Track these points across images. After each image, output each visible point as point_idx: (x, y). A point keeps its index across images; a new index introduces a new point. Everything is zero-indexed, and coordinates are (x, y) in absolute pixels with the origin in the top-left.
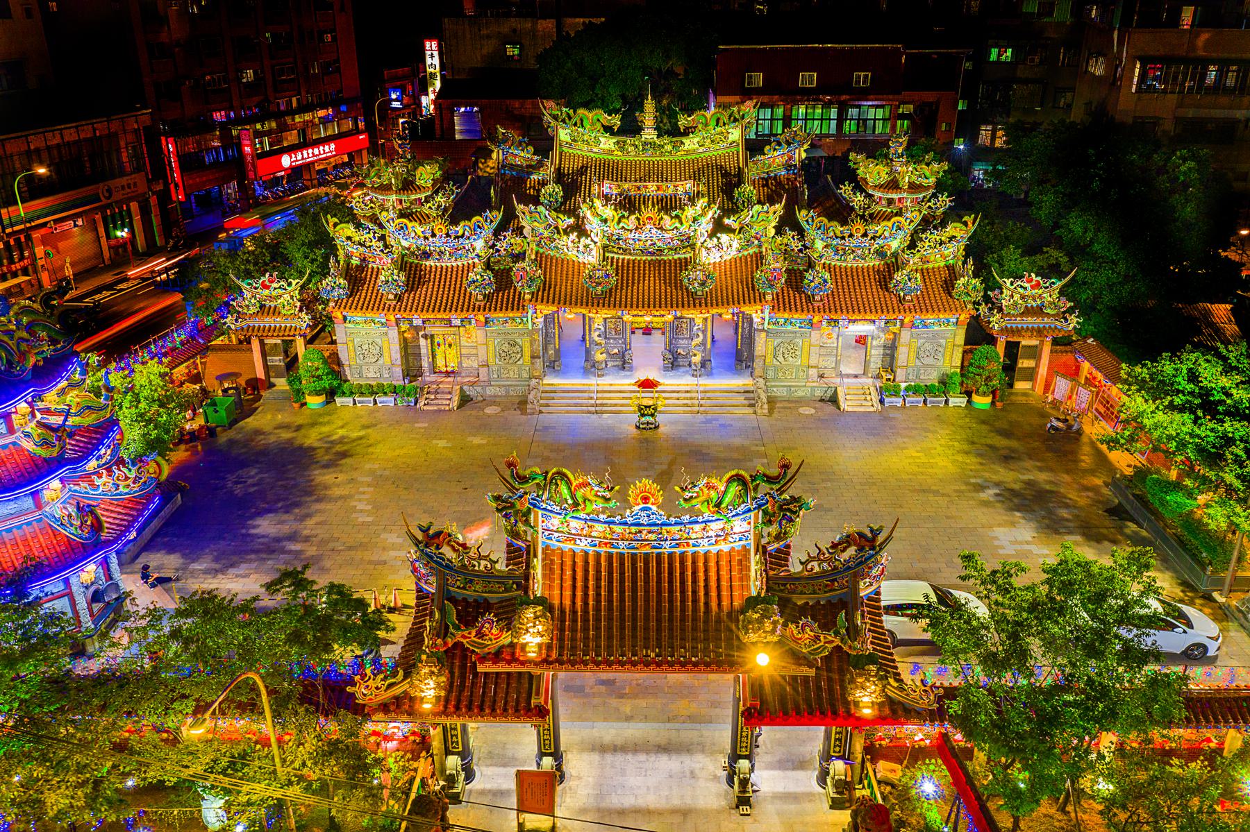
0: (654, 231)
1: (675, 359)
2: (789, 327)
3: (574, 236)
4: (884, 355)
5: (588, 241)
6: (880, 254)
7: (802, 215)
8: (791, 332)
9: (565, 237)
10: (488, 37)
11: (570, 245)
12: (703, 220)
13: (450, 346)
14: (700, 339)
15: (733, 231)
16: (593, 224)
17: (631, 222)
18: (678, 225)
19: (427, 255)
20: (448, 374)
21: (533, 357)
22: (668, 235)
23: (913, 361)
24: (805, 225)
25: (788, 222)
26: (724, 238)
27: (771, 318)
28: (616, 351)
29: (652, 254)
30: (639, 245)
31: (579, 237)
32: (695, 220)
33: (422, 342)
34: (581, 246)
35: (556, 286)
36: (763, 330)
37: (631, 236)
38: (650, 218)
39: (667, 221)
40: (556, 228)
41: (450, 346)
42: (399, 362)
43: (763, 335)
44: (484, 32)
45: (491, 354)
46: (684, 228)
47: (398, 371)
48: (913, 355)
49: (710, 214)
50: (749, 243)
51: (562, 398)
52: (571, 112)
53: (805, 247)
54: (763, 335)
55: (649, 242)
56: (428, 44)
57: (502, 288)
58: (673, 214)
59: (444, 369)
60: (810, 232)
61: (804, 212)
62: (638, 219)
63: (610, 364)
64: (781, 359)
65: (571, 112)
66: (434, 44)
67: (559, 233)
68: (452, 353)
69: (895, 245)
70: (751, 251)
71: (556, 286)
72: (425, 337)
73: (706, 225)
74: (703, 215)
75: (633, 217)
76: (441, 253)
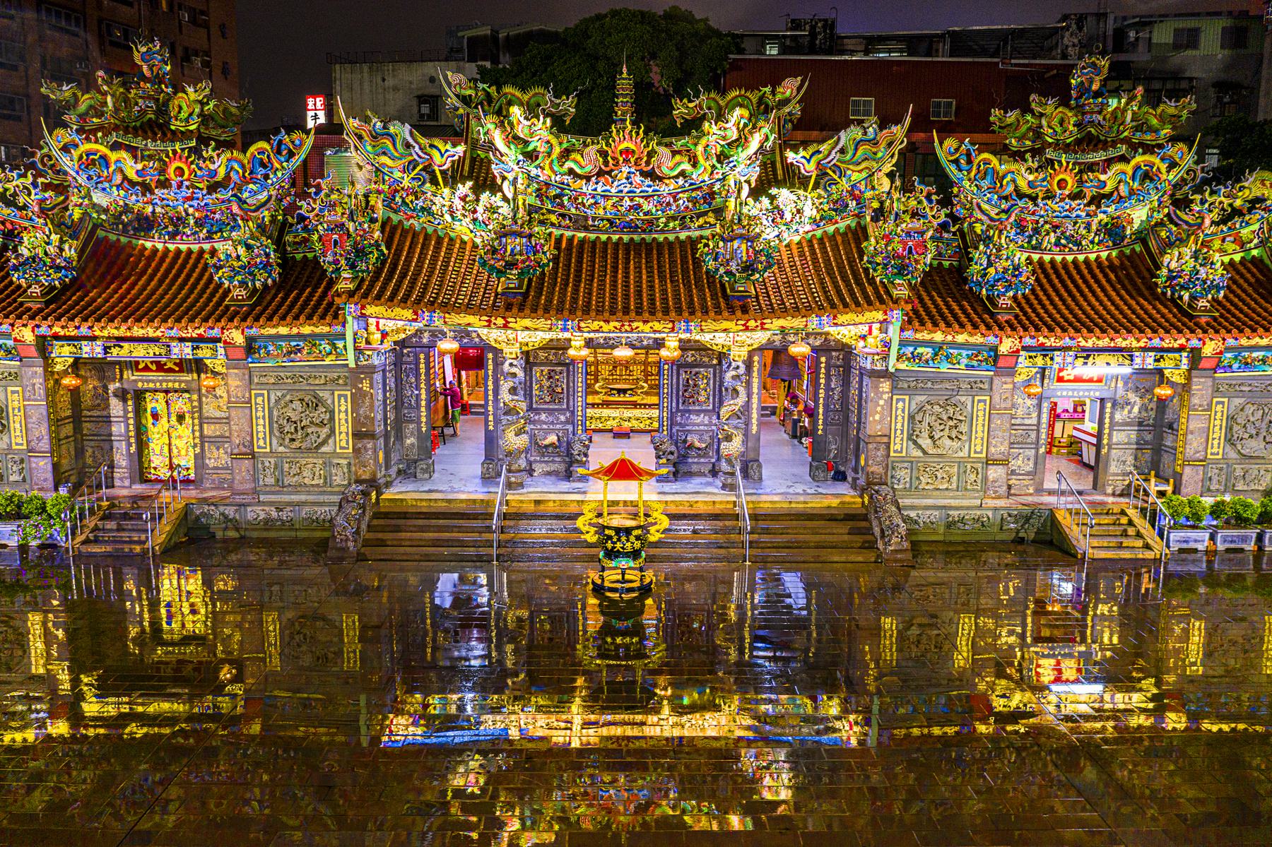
0: (638, 179)
1: (683, 458)
2: (944, 368)
3: (464, 188)
4: (1140, 445)
5: (497, 200)
6: (1113, 231)
7: (946, 148)
8: (949, 379)
9: (447, 191)
10: (396, 89)
11: (458, 204)
12: (742, 156)
13: (181, 418)
14: (742, 399)
15: (804, 182)
16: (508, 161)
17: (587, 160)
18: (686, 166)
19: (145, 224)
20: (171, 483)
21: (357, 435)
22: (665, 189)
23: (1217, 448)
24: (951, 170)
25: (917, 166)
26: (785, 196)
27: (903, 343)
28: (552, 438)
29: (631, 227)
30: (605, 209)
31: (477, 190)
32: (722, 158)
33: (116, 407)
34: (480, 209)
35: (404, 263)
36: (885, 374)
37: (587, 188)
38: (627, 152)
39: (666, 162)
40: (428, 169)
41: (181, 418)
42: (45, 445)
43: (885, 386)
44: (390, 82)
45: (261, 428)
46: (700, 175)
47: (42, 467)
48: (1218, 434)
49: (754, 143)
50: (840, 207)
51: (422, 529)
52: (493, 90)
53: (954, 218)
54: (885, 386)
55: (627, 203)
56: (310, 102)
57: (298, 286)
58: (679, 144)
59: (164, 473)
60: (966, 186)
61: (950, 143)
62: (604, 154)
63: (539, 469)
64: (925, 442)
65: (493, 90)
66: (319, 101)
67: (434, 182)
68: (184, 437)
69: (1139, 215)
70: (842, 226)
71: (404, 263)
72: (122, 395)
73: (744, 168)
74: (741, 141)
75: (592, 150)
76: (179, 221)
